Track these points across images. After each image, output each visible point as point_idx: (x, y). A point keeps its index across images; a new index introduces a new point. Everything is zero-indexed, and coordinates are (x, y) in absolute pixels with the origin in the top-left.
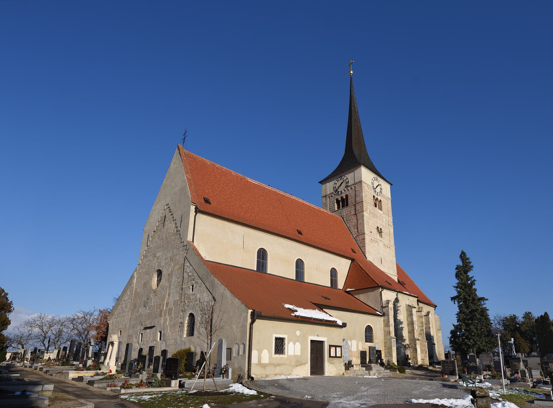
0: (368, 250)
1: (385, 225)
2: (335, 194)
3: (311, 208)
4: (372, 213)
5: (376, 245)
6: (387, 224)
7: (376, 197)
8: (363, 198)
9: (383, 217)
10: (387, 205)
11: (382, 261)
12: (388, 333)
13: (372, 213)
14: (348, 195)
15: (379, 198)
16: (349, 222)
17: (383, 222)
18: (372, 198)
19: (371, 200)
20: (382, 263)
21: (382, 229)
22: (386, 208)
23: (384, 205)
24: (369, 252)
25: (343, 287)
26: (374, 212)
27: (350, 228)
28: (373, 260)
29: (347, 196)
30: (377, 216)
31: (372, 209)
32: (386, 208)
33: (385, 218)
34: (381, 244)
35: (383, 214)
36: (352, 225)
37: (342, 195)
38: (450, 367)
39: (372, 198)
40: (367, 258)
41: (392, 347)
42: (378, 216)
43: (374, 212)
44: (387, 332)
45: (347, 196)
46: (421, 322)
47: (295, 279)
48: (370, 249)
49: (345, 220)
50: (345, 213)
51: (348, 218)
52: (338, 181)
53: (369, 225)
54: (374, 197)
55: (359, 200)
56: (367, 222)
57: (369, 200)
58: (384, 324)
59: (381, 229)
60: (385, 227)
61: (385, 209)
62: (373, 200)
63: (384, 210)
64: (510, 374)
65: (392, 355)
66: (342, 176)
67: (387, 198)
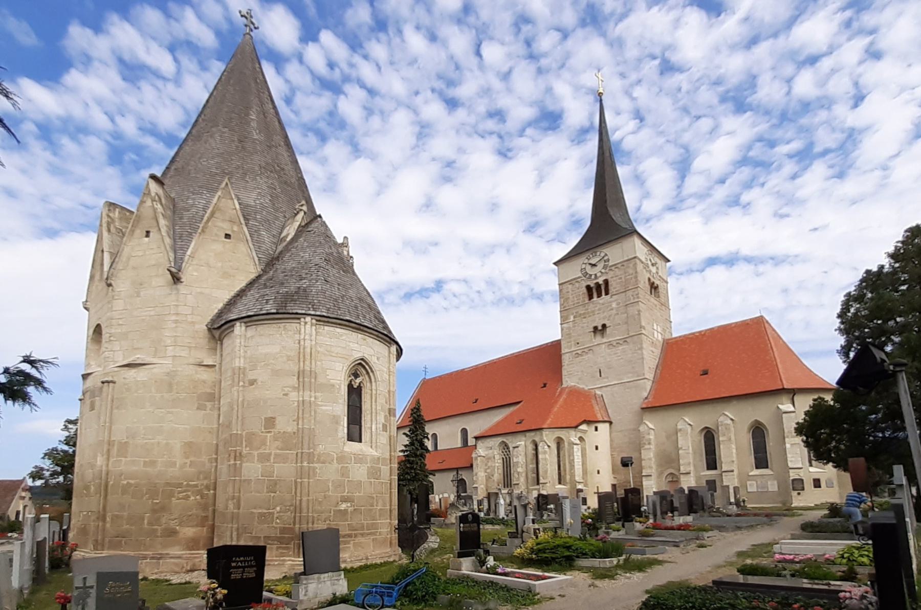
5: (590, 355)
7: (652, 280)
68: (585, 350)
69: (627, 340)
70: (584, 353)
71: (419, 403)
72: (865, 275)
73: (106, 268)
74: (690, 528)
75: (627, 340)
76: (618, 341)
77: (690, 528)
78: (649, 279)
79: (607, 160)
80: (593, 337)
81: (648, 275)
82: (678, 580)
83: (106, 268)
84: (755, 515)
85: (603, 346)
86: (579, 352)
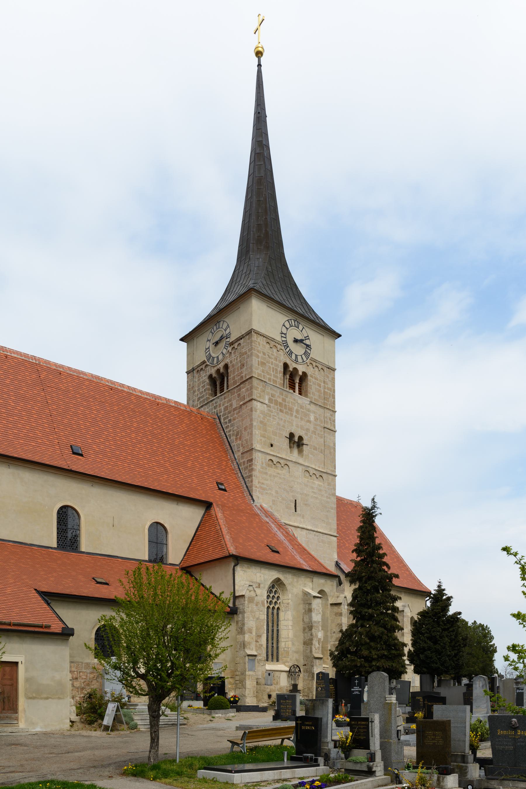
0: (259, 482)
1: (315, 428)
2: (208, 364)
3: (133, 398)
4: (276, 403)
5: (285, 471)
6: (318, 428)
7: (292, 365)
8: (254, 370)
9: (309, 410)
10: (322, 384)
11: (297, 505)
12: (242, 645)
13: (276, 403)
14: (230, 365)
15: (301, 369)
16: (229, 424)
17: (309, 421)
18: (279, 369)
19: (277, 373)
20: (297, 510)
21: (305, 437)
22: (319, 391)
23: (314, 384)
24: (261, 487)
25: (182, 561)
26: (284, 400)
27: (230, 438)
28: (273, 504)
29: (226, 367)
30: (291, 409)
31: (277, 394)
32: (319, 391)
33: (314, 413)
34: (298, 471)
35: (309, 404)
36: (233, 431)
37: (218, 367)
38: (288, 706)
39: (281, 369)
40: (254, 501)
41: (245, 671)
42: (295, 408)
43: (284, 400)
44: (241, 644)
45: (226, 367)
46: (338, 624)
47: (55, 545)
48: (266, 482)
49: (222, 421)
50: (223, 405)
51: (228, 417)
52: (213, 333)
53: (265, 430)
54: (286, 366)
55: (246, 375)
56: (261, 422)
57: (269, 374)
58: (237, 630)
59: (301, 438)
60: (314, 432)
61: (317, 393)
62: (282, 374)
63: (314, 395)
64: (407, 717)
65: (245, 685)
66: (220, 322)
67: (324, 368)
68: (282, 461)
69: (324, 475)
70: (278, 465)
71: (374, 502)
72: (470, 624)
73: (54, 755)
74: (326, 762)
75: (324, 475)
76: (321, 474)
77: (326, 762)
78: (286, 366)
79: (260, 80)
80: (289, 452)
81: (283, 358)
82: (195, 341)
83: (54, 755)
84: (273, 624)
85: (301, 468)
86: (275, 460)
